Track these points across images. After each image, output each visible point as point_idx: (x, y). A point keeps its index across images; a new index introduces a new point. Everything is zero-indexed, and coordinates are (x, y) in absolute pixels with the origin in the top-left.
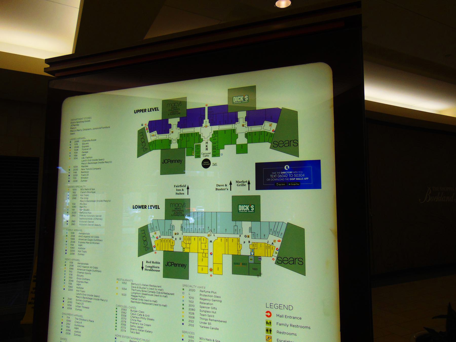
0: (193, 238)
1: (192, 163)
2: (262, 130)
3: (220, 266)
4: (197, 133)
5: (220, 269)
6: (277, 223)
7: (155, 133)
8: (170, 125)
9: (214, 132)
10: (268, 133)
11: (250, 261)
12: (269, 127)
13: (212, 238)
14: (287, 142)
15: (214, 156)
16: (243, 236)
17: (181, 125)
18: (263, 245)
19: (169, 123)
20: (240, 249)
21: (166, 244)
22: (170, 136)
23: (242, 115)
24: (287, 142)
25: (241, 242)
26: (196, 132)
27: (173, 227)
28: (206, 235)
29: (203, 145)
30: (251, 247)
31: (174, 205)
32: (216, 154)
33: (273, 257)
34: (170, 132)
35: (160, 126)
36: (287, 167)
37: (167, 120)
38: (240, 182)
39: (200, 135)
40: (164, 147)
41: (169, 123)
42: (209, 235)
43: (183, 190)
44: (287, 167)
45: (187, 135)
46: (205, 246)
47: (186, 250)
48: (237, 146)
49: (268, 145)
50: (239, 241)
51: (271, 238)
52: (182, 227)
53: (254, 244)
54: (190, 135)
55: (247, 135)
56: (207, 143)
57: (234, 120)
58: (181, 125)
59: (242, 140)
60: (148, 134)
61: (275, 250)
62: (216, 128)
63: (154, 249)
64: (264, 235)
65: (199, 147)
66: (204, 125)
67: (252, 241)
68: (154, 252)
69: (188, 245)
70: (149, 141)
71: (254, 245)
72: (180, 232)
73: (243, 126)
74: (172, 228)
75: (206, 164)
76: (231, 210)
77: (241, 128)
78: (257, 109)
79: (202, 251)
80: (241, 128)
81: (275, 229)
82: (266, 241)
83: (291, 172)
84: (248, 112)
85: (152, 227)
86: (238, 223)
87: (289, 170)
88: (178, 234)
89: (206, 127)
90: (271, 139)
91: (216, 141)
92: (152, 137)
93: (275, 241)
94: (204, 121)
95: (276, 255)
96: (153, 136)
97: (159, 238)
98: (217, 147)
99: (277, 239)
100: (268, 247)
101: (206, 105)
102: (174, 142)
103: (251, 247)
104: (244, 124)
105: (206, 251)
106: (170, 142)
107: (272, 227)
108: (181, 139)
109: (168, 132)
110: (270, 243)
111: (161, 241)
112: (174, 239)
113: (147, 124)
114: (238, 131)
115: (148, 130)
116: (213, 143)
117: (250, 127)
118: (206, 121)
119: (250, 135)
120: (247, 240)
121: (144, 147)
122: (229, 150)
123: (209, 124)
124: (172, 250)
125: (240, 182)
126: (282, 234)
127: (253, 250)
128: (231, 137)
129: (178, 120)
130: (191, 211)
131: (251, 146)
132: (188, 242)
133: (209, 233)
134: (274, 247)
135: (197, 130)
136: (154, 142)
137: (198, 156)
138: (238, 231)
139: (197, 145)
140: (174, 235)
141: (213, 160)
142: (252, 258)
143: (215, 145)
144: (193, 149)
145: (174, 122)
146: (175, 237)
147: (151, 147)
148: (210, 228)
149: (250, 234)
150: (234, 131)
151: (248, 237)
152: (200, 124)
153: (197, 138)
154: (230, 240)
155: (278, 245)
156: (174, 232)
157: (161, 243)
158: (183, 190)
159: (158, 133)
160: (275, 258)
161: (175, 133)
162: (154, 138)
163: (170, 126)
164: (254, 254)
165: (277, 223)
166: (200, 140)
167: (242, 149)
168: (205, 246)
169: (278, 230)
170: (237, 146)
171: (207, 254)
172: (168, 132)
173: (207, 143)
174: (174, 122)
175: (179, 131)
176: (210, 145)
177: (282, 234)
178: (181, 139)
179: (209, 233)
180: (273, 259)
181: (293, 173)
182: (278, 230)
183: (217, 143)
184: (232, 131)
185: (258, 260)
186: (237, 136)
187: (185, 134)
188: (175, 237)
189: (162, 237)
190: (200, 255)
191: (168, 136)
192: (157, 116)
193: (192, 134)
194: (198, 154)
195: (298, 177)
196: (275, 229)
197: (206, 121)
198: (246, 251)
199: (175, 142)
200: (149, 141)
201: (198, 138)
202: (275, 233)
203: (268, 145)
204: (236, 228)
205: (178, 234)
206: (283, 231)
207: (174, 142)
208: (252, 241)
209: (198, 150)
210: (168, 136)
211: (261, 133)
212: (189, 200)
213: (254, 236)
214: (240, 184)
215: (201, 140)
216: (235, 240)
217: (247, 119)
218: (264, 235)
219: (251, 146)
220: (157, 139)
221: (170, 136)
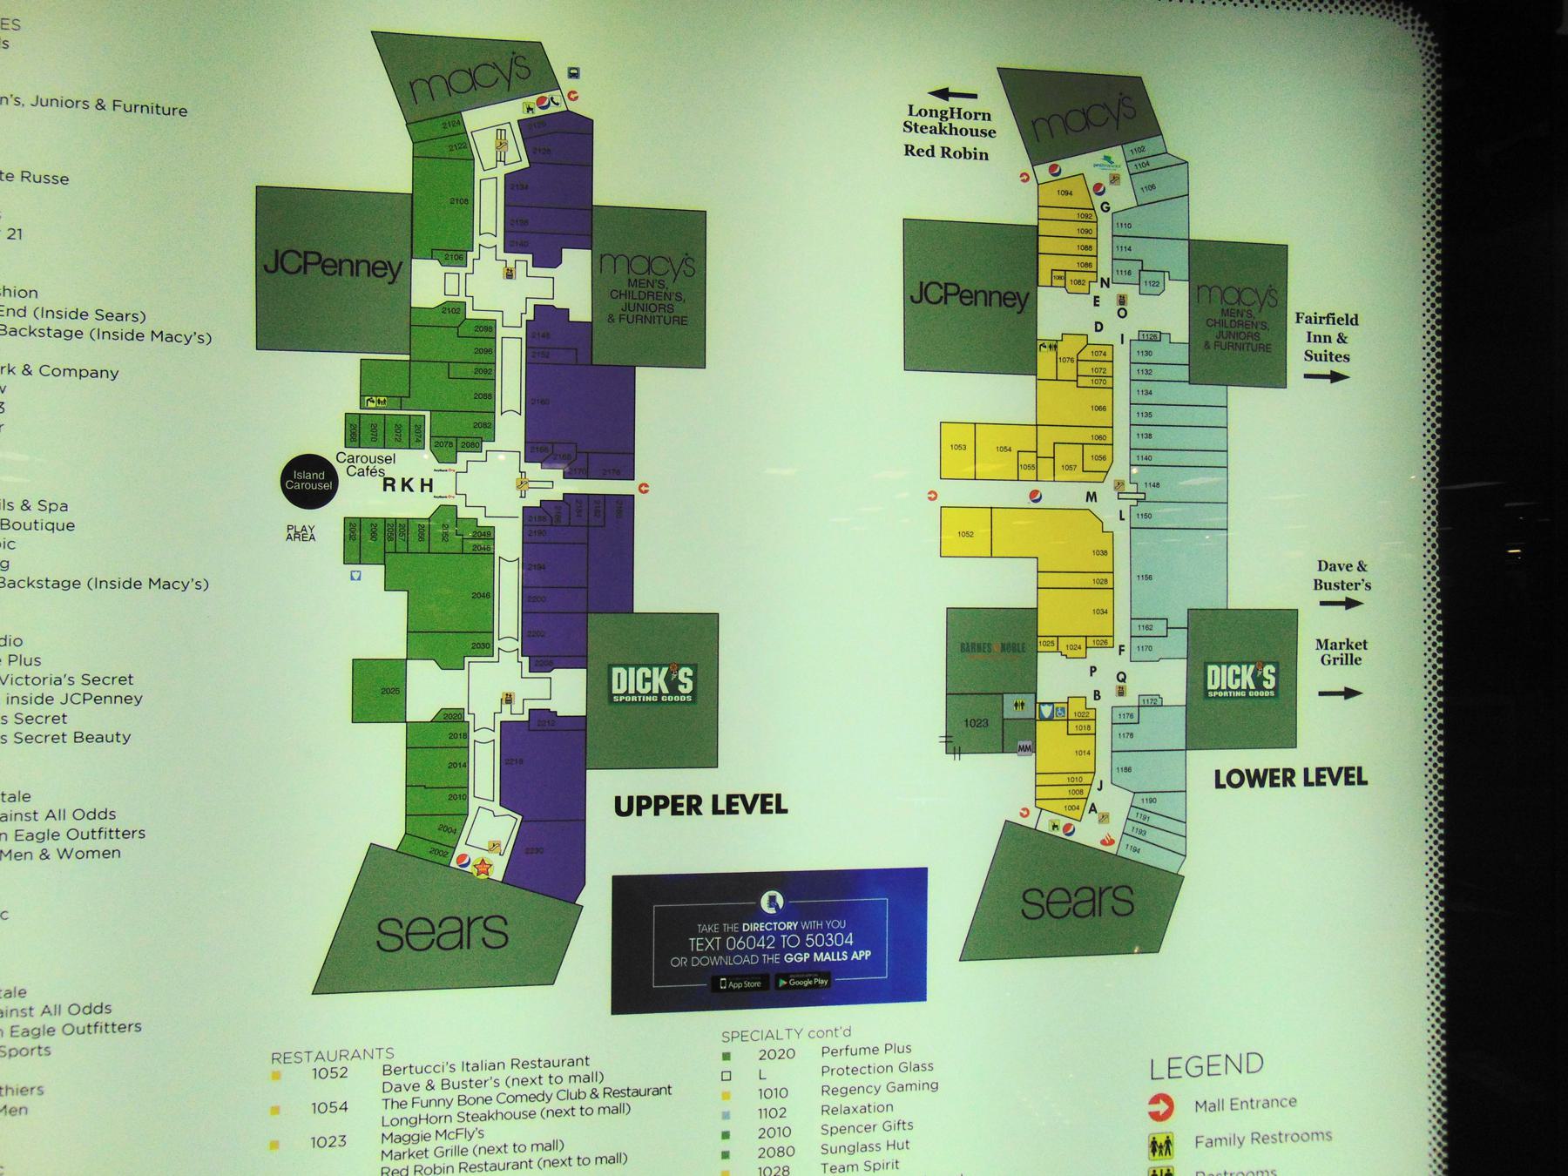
0: (1102, 397)
1: (318, 394)
2: (473, 804)
3: (980, 544)
4: (490, 426)
5: (966, 545)
6: (1179, 828)
7: (517, 158)
8: (555, 262)
9: (488, 534)
10: (456, 832)
11: (1009, 700)
12: (490, 833)
13: (1109, 506)
14: (1088, 894)
15: (354, 528)
16: (1122, 663)
17: (547, 326)
18: (1084, 764)
19: (567, 253)
20: (1062, 648)
21: (1071, 246)
22: (487, 255)
23: (566, 692)
24: (455, 925)
25: (1095, 656)
26: (501, 422)
27: (1156, 288)
28: (1120, 470)
29: (415, 462)
30: (1076, 707)
31: (1216, 293)
32: (366, 540)
33: (1034, 812)
34: (511, 257)
35: (554, 197)
36: (772, 899)
37: (582, 240)
38: (1334, 646)
39: (474, 445)
40: (428, 218)
41: (567, 253)
42: (1119, 485)
43: (1341, 339)
44: (772, 899)
45: (487, 371)
46: (1069, 468)
47: (1045, 359)
48: (397, 668)
49: (391, 834)
50: (1103, 642)
51: (1115, 802)
52: (1155, 337)
53: (1088, 717)
54: (483, 387)
55: (453, 719)
56: (427, 485)
57: (543, 653)
58: (547, 326)
59: (429, 690)
60: (512, 111)
61: (1063, 822)
62: (509, 543)
63: (1043, 171)
64: (1128, 770)
65: (410, 437)
66: (534, 470)
67: (1103, 710)
68: (1028, 168)
69: (1067, 371)
70: (474, 119)
71: (1082, 717)
72: (1131, 327)
73: (509, 699)
74: (1150, 280)
75: (308, 481)
76: (1236, 603)
77: (499, 686)
78: (591, 775)
79: (1045, 450)
80: (499, 686)
81: (1154, 820)
82: (1103, 773)
83: (789, 925)
84: (577, 725)
85: (1154, 163)
86: (1179, 640)
87: (782, 915)
88: (1122, 313)
89: (523, 484)
90: (423, 849)
91: (437, 546)
92: (494, 133)
93: (1104, 818)
94: (556, 474)
95: (1044, 826)
96: (501, 145)
97: (1098, 200)
98: (402, 547)
99: (1114, 829)
100: (1078, 786)
101: (644, 488)
102: (452, 280)
103: (1076, 707)
104: (517, 707)
105: (1045, 465)
106: (455, 255)
107: (1164, 804)
108: (463, 331)
109: (513, 244)
110: (1095, 797)
111: (1087, 216)
112: (1096, 289)
113: (574, 107)
114: (479, 668)
115: (539, 112)
116: (422, 528)
117: (497, 736)
118: (554, 484)
119: (453, 736)
120: (1108, 687)
121: (435, 77)
122: (376, 617)
123: (533, 500)
124: (1044, 277)
125: (1334, 646)
126: (1136, 850)
127: (1060, 712)
128: (450, 635)
129: (581, 311)
130: (1234, 391)
131: (393, 737)
132: (1085, 368)
133: (1130, 488)
134: (1076, 814)
135: (511, 428)
136: (461, 150)
137: (356, 431)
138: (1145, 629)
139: (420, 430)
140: (1116, 290)
141: (328, 520)
142: (1028, 712)
143: (414, 536)
144: (401, 401)
145: (572, 284)
146: (1109, 296)
147: (436, 128)
148: (1152, 494)
149: (1131, 699)
150: (484, 648)
151: (1121, 692)
152: (538, 449)
153: (463, 425)
154: (1102, 599)
155: (1088, 833)
156: (1131, 292)
157: (1073, 214)
158: (1341, 339)
159: (513, 183)
160: (1029, 822)
161: (500, 289)
162: (484, 145)
163: (548, 258)
164: (1043, 719)
165: (1179, 828)
166: (447, 447)
167: (377, 691)
168: (1069, 468)
169: (1152, 835)
170: (397, 668)
171: (1031, 474)
172: (513, 244)
173: (427, 485)
174: (572, 284)
175: (513, 318)
176: (417, 506)
177: (1136, 850)
178: (463, 331)
179: (1130, 488)
180: (1025, 813)
181: (800, 931)
182: (1152, 835)
183: (423, 547)
184: (483, 638)
185: (1015, 737)
186: (451, 662)
187: (491, 351)
188: (1109, 296)
189: (1104, 220)
190: (1025, 439)
191: (488, 240)
192: (616, 182)
193: (490, 396)
194: (366, 433)
195: (825, 949)
196: (1154, 820)
197: (554, 484)
198: (1056, 678)
199: (452, 289)
200: (474, 119)
201: (465, 435)
202: (1140, 819)
203: (391, 834)
204: (1159, 628)
205: (1122, 313)
206: (1148, 856)
207: (452, 280)
208: (1103, 710)
209: (391, 436)
210: (488, 240)
211: (460, 794)
212: (1278, 379)
213: (1126, 720)
214: (1336, 653)
215: (447, 452)
216: (1100, 626)
217: (543, 719)
218: (1128, 770)
219: (393, 737)
220: (479, 174)
221: (487, 255)
